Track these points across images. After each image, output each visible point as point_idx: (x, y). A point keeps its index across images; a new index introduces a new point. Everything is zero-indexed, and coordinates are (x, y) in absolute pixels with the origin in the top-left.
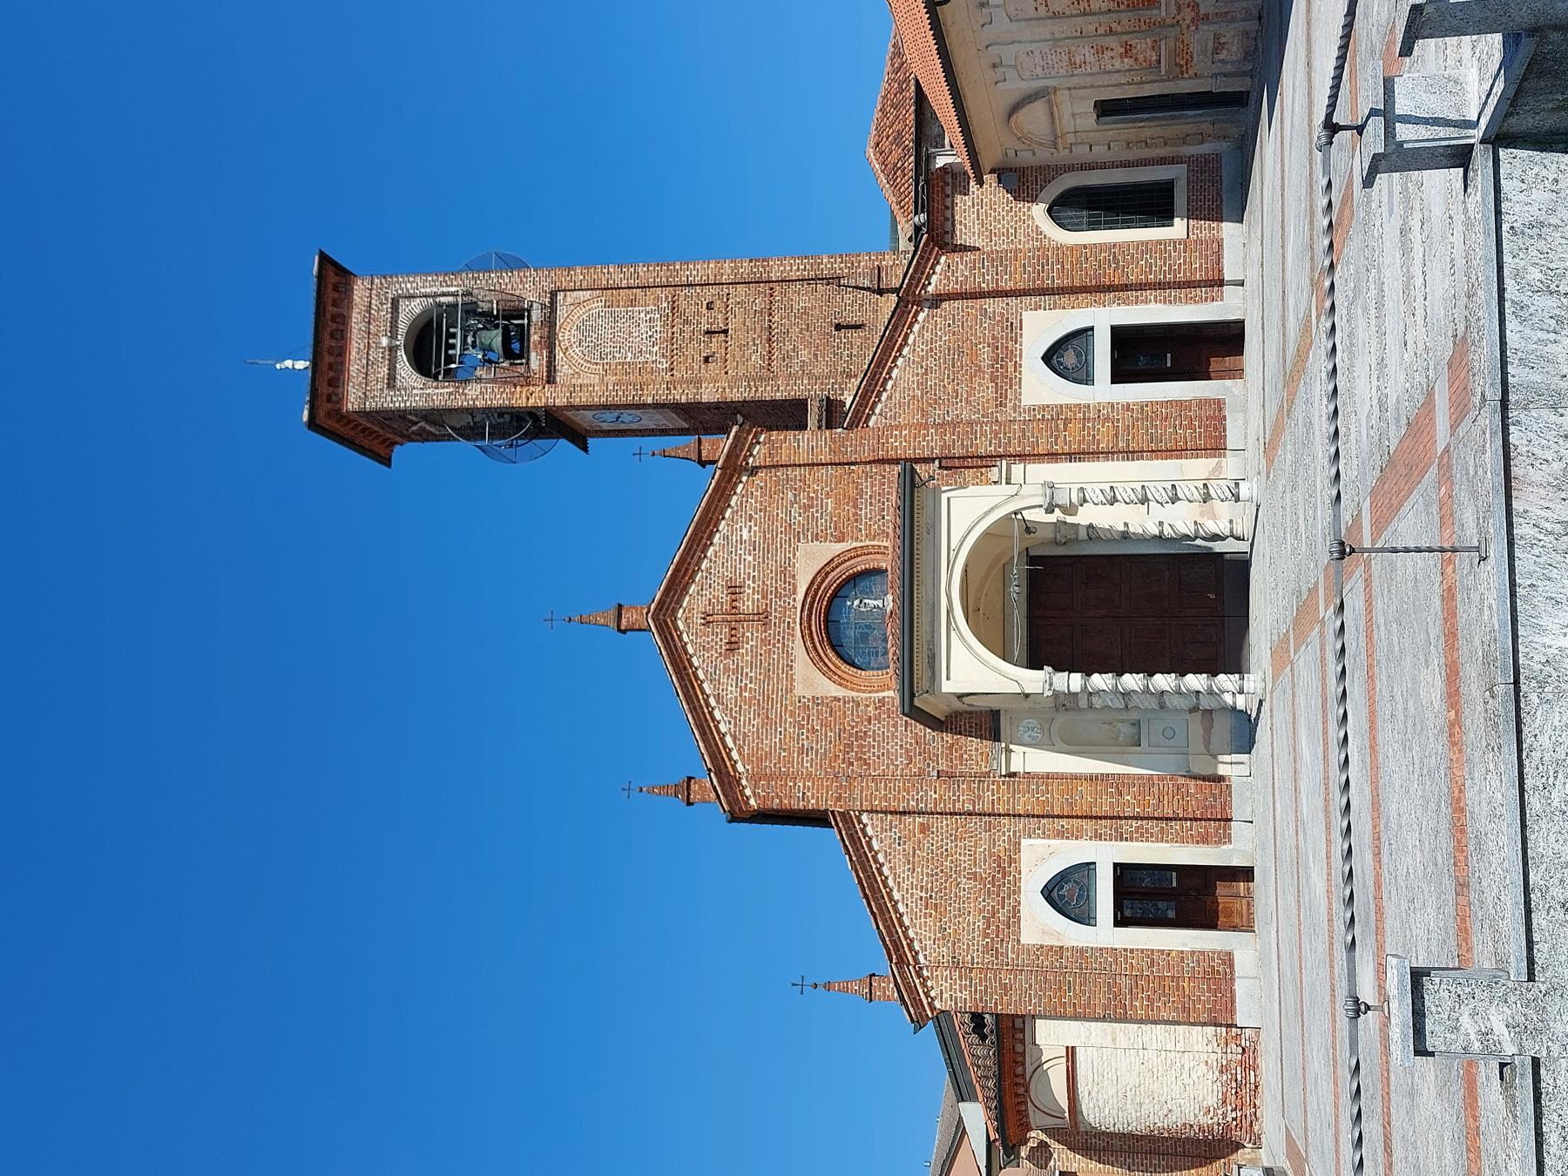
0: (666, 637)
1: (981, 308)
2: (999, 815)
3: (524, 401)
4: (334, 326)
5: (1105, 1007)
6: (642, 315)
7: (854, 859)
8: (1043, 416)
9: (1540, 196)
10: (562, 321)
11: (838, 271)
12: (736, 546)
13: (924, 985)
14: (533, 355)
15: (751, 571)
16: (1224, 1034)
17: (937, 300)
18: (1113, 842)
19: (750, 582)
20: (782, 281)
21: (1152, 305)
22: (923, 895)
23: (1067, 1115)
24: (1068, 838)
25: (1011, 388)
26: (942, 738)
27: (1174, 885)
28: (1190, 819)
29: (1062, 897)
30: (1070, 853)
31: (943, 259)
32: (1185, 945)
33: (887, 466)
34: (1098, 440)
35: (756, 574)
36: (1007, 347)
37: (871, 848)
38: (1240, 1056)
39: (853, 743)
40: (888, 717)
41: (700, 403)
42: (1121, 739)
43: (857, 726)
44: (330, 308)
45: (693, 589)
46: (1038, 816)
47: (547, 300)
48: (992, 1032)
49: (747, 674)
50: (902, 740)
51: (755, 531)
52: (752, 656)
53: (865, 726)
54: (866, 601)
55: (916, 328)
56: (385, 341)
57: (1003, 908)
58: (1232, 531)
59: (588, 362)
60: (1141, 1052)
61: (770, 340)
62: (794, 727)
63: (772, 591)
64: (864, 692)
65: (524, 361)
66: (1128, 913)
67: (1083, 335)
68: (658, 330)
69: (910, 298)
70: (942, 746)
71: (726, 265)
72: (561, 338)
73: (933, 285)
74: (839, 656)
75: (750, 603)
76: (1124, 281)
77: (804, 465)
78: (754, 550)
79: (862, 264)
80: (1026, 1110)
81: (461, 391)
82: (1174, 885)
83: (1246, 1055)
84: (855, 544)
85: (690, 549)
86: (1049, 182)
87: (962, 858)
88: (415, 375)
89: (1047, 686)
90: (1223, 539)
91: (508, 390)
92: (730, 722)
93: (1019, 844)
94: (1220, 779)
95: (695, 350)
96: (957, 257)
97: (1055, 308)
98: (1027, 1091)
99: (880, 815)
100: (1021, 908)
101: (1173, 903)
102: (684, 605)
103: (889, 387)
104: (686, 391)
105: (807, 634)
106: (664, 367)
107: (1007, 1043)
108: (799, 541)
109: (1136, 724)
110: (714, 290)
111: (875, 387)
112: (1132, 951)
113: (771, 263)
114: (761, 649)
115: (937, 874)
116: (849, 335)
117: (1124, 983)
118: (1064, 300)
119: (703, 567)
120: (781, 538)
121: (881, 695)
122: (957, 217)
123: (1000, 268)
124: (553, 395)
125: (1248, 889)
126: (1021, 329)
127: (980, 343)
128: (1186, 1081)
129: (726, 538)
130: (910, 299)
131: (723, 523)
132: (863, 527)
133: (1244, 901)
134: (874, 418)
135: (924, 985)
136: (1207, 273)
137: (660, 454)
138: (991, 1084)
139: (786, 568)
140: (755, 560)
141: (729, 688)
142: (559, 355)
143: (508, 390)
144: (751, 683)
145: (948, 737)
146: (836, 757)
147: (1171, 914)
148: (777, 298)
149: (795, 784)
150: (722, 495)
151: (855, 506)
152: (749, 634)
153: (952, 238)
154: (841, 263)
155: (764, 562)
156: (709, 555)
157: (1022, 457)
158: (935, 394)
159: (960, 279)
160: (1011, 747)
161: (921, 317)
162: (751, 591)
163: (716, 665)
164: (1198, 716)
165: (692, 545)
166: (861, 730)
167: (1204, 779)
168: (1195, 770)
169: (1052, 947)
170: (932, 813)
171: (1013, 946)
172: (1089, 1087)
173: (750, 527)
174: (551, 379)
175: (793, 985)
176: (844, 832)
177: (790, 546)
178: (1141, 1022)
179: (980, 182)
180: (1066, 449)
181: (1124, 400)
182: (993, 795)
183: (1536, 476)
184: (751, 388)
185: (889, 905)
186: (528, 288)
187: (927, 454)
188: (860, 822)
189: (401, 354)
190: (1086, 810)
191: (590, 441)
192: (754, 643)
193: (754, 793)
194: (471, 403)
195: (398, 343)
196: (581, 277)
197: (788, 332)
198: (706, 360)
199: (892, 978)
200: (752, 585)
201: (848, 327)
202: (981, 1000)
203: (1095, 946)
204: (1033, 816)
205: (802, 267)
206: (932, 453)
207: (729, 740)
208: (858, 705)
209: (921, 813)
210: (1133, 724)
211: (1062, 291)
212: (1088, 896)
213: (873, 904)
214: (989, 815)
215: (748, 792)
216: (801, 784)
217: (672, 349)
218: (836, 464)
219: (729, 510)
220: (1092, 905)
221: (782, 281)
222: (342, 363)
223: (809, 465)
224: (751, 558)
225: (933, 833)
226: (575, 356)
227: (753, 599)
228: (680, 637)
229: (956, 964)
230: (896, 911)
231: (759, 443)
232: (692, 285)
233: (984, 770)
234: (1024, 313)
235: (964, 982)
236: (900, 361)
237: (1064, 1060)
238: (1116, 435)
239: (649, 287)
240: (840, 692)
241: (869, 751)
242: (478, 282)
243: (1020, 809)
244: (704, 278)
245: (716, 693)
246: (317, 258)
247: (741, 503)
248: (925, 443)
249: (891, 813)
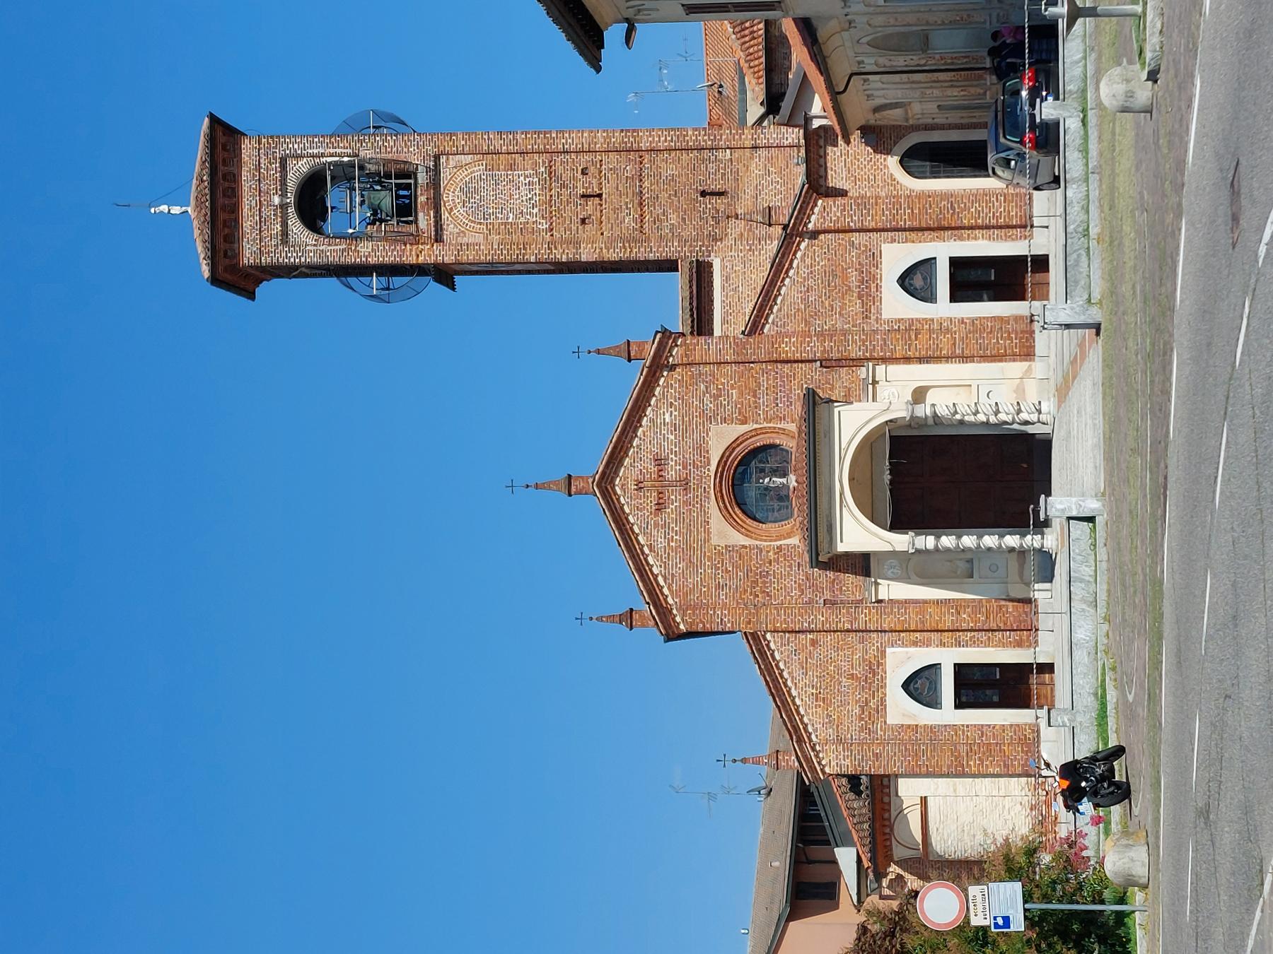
0: (608, 501)
1: (850, 240)
2: (870, 631)
3: (415, 258)
4: (227, 184)
5: (949, 766)
6: (522, 178)
7: (763, 667)
8: (899, 327)
9: (1079, 532)
10: (446, 183)
11: (702, 143)
12: (661, 428)
13: (817, 756)
14: (421, 215)
15: (673, 447)
16: (1033, 782)
17: (814, 235)
18: (954, 649)
19: (673, 456)
20: (651, 150)
21: (980, 242)
22: (814, 691)
23: (921, 847)
24: (920, 646)
25: (874, 304)
26: (826, 575)
27: (998, 677)
28: (1009, 630)
29: (916, 689)
30: (920, 657)
31: (820, 202)
32: (1005, 720)
33: (779, 365)
34: (941, 348)
35: (677, 449)
36: (870, 272)
37: (774, 659)
38: (1044, 798)
39: (758, 579)
40: (785, 560)
41: (580, 261)
42: (959, 573)
43: (760, 567)
44: (222, 168)
45: (627, 461)
46: (899, 631)
47: (432, 163)
48: (867, 788)
49: (673, 528)
50: (795, 577)
51: (675, 416)
52: (676, 515)
53: (767, 568)
54: (774, 479)
55: (799, 255)
56: (277, 200)
57: (874, 699)
58: (1039, 419)
59: (472, 222)
60: (974, 798)
61: (642, 204)
62: (712, 569)
63: (690, 463)
64: (765, 541)
65: (411, 219)
66: (964, 699)
67: (928, 264)
68: (537, 192)
69: (795, 233)
70: (827, 581)
71: (599, 134)
72: (445, 199)
73: (813, 222)
74: (744, 512)
75: (673, 473)
76: (959, 224)
77: (714, 363)
78: (675, 430)
79: (723, 137)
80: (891, 845)
81: (353, 248)
82: (998, 677)
83: (1049, 796)
84: (756, 426)
85: (625, 430)
86: (901, 139)
87: (843, 663)
88: (307, 232)
89: (911, 546)
90: (1033, 424)
91: (398, 248)
92: (661, 566)
93: (885, 652)
94: (1028, 601)
95: (572, 212)
96: (830, 201)
97: (906, 242)
98: (892, 830)
99: (780, 634)
100: (887, 699)
101: (997, 691)
102: (620, 475)
103: (779, 302)
104: (566, 251)
105: (719, 497)
106: (544, 227)
107: (878, 795)
108: (711, 423)
109: (970, 561)
110: (587, 157)
111: (768, 302)
112: (968, 726)
113: (640, 134)
114: (683, 508)
115: (824, 676)
116: (714, 201)
117: (963, 750)
118: (913, 235)
119: (634, 444)
120: (697, 421)
121: (779, 543)
122: (828, 165)
123: (864, 211)
124: (442, 253)
125: (1052, 678)
126: (881, 258)
127: (849, 268)
128: (1007, 817)
129: (652, 420)
130: (793, 234)
131: (650, 408)
132: (761, 412)
133: (1049, 687)
134: (767, 326)
135: (817, 756)
136: (1021, 220)
137: (595, 352)
138: (866, 826)
139: (701, 445)
140: (676, 439)
141: (659, 540)
142: (445, 215)
143: (398, 248)
144: (676, 535)
145: (831, 574)
146: (745, 591)
147: (996, 699)
148: (646, 166)
149: (715, 612)
150: (649, 386)
151: (755, 396)
152: (673, 497)
153: (825, 181)
154: (705, 135)
155: (683, 440)
156: (638, 434)
157: (884, 360)
158: (815, 308)
159: (833, 219)
160: (879, 581)
161: (803, 246)
162: (673, 463)
163: (648, 522)
164: (1014, 555)
165: (626, 428)
166: (764, 571)
167: (1019, 601)
168: (1013, 595)
169: (909, 725)
170: (820, 631)
171: (881, 726)
172: (937, 825)
173: (671, 412)
174: (438, 239)
175: (718, 761)
176: (754, 648)
177: (704, 427)
178: (974, 776)
179: (848, 142)
180: (917, 355)
181: (960, 316)
182: (866, 617)
183: (1076, 598)
184: (626, 249)
185: (789, 700)
186: (414, 153)
187: (811, 356)
188: (765, 639)
189: (291, 210)
190: (934, 626)
191: (457, 279)
192: (678, 504)
193: (683, 619)
194: (364, 259)
195: (288, 201)
196: (463, 143)
197: (658, 197)
198: (583, 221)
199: (794, 752)
200: (674, 458)
201: (713, 194)
202: (859, 766)
203: (941, 723)
204: (895, 631)
205: (669, 138)
206: (815, 356)
207: (660, 579)
208: (761, 551)
209: (811, 631)
210: (968, 561)
211: (912, 229)
212: (936, 688)
213: (777, 699)
214: (863, 631)
215: (678, 619)
216: (719, 613)
217: (550, 210)
218: (739, 363)
219: (654, 399)
220: (939, 694)
221: (651, 150)
222: (236, 221)
223: (717, 363)
224: (673, 437)
225: (820, 646)
226: (460, 216)
227: (676, 470)
228: (618, 499)
229: (840, 741)
230: (794, 704)
231: (677, 345)
232: (567, 152)
233: (858, 598)
234: (883, 245)
235: (846, 754)
236: (787, 280)
237: (919, 806)
238: (954, 344)
239: (527, 153)
240: (746, 541)
241: (771, 586)
242: (364, 144)
243: (886, 627)
244: (579, 146)
245: (648, 543)
246: (207, 121)
247: (664, 392)
248: (809, 348)
249: (789, 632)
